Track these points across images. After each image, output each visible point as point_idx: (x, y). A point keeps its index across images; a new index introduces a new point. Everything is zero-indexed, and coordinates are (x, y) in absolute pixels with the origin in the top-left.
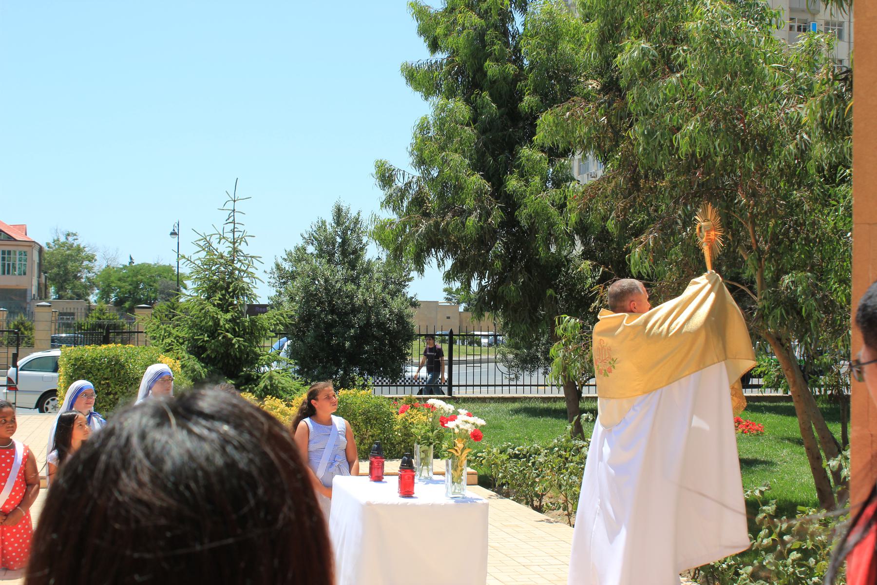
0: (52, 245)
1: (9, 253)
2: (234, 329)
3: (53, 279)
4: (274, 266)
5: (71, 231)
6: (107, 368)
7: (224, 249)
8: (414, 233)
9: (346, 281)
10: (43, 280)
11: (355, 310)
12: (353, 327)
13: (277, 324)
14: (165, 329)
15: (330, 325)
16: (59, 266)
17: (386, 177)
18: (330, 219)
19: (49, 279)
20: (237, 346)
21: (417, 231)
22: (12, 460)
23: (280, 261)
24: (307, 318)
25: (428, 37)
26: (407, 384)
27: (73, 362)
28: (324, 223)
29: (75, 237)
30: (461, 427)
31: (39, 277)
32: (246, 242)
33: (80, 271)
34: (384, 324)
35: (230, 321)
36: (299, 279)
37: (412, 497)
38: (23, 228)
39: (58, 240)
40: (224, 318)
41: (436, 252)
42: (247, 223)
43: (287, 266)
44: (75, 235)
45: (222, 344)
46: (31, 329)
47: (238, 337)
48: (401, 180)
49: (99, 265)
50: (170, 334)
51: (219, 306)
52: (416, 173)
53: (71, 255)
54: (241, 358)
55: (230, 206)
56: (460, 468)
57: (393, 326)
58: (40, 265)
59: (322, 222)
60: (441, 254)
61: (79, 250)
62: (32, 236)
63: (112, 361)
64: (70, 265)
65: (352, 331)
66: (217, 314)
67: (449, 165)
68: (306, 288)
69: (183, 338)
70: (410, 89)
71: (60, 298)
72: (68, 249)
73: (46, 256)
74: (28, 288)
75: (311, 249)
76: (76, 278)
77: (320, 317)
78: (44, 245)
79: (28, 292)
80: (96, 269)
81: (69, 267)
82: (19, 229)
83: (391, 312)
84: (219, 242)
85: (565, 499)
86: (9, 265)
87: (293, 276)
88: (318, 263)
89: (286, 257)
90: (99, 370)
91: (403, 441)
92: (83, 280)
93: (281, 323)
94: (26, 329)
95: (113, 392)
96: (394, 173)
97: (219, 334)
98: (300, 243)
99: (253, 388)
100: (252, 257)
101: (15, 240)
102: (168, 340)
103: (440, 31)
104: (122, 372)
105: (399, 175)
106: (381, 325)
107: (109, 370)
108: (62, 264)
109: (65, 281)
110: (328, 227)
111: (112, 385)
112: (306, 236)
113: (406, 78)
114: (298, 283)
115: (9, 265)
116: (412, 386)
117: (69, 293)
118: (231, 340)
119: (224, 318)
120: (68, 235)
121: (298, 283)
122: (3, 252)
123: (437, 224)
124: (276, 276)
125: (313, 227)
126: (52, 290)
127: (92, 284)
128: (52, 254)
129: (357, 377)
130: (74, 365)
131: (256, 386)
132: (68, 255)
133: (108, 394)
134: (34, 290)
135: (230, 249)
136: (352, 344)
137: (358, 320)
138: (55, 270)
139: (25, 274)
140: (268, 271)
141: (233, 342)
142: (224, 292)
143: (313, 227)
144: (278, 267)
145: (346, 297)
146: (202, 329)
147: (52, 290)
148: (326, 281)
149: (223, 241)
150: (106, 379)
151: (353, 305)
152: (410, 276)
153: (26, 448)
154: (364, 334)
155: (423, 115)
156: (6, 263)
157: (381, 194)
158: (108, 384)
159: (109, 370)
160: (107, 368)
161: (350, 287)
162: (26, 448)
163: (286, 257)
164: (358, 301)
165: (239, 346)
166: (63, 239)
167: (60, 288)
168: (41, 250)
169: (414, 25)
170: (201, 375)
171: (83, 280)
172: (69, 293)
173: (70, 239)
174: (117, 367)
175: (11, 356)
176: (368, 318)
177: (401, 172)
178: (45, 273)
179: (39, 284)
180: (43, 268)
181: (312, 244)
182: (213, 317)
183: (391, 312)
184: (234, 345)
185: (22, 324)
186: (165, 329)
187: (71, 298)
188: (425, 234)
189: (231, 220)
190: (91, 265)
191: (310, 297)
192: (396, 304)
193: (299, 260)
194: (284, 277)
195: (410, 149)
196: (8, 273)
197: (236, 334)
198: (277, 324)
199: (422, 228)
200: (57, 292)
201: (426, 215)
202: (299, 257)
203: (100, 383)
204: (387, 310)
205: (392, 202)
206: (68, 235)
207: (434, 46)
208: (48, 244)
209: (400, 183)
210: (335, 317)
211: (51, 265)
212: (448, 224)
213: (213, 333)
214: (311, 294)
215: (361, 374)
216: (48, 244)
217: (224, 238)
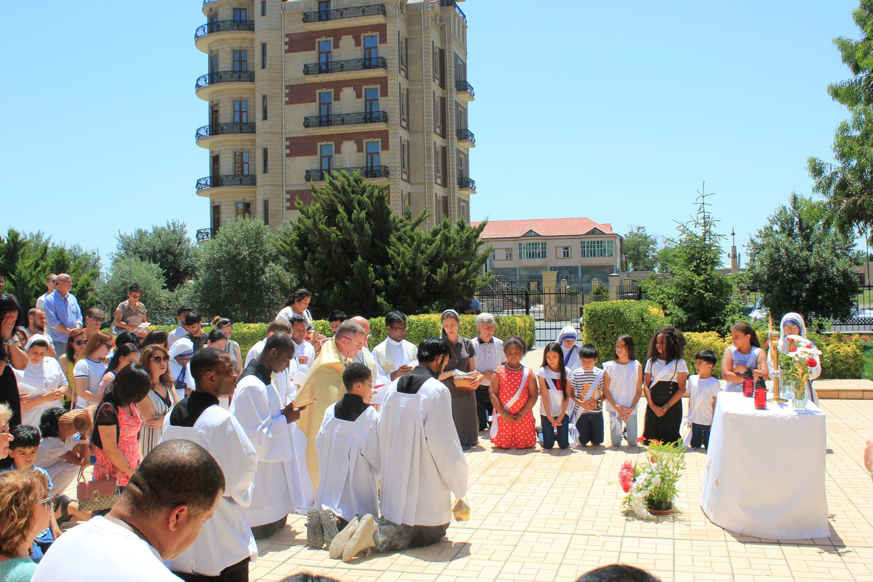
0: (628, 236)
1: (601, 242)
2: (706, 287)
3: (630, 258)
4: (749, 241)
5: (640, 226)
6: (611, 316)
7: (699, 232)
8: (837, 210)
9: (802, 249)
10: (624, 259)
11: (809, 270)
12: (808, 282)
13: (739, 282)
14: (660, 289)
15: (791, 282)
16: (634, 249)
17: (817, 170)
18: (789, 206)
19: (628, 258)
20: (707, 299)
21: (839, 208)
22: (522, 376)
23: (753, 237)
24: (774, 277)
25: (851, 62)
26: (867, 323)
27: (589, 312)
28: (784, 208)
29: (644, 230)
30: (800, 356)
31: (621, 257)
32: (714, 225)
33: (647, 252)
34: (833, 279)
35: (703, 281)
36: (766, 249)
37: (765, 409)
38: (609, 226)
39: (632, 232)
40: (697, 279)
41: (857, 224)
42: (714, 213)
43: (759, 241)
44: (643, 228)
45: (698, 298)
46: (607, 291)
47: (709, 292)
48: (829, 171)
49: (660, 246)
50: (663, 292)
51: (694, 271)
52: (838, 164)
53: (641, 241)
54: (711, 307)
55: (701, 200)
56: (801, 388)
57: (840, 280)
58: (621, 249)
59: (783, 207)
60: (861, 224)
61: (646, 237)
62: (615, 231)
63: (615, 311)
64: (641, 248)
65: (807, 285)
66: (692, 277)
67: (865, 156)
68: (771, 256)
69: (672, 294)
70: (837, 103)
71: (636, 270)
72: (639, 238)
73: (625, 243)
74: (615, 265)
75: (776, 228)
76: (645, 256)
77: (783, 276)
78: (623, 236)
79: (615, 267)
80: (657, 250)
81: (640, 250)
82: (607, 227)
83: (838, 270)
84: (696, 226)
85: (190, 444)
86: (601, 250)
87: (763, 247)
88: (782, 237)
89: (758, 234)
90: (606, 317)
91: (832, 366)
92: (650, 258)
93: (742, 282)
94: (604, 291)
95: (617, 332)
96: (823, 166)
97: (695, 291)
98: (768, 224)
99: (720, 328)
100: (719, 235)
101: (605, 234)
102: (662, 296)
103: (859, 54)
104: (622, 318)
105: (827, 168)
106: (830, 280)
107: (613, 317)
108: (636, 247)
109: (638, 259)
110: (788, 211)
111: (615, 327)
112: (771, 219)
113: (832, 95)
114: (764, 253)
115: (601, 250)
116: (853, 325)
117: (641, 267)
118: (704, 294)
119: (697, 279)
120: (639, 228)
121: (764, 253)
122: (582, 242)
123: (855, 202)
124: (751, 248)
125: (777, 212)
126: (630, 265)
127: (656, 260)
128: (629, 241)
129: (812, 319)
130: (590, 314)
131: (723, 326)
132: (639, 242)
133: (613, 333)
134: (618, 266)
135: (704, 231)
136: (807, 294)
137: (812, 277)
138: (632, 252)
139: (612, 255)
140: (746, 245)
141: (705, 296)
142: (698, 261)
143: (777, 212)
144: (752, 241)
145: (803, 261)
146: (684, 287)
147: (630, 265)
148: (786, 249)
149: (698, 225)
150: (611, 323)
151: (808, 266)
152: (854, 243)
153: (531, 371)
154: (817, 287)
155: (843, 120)
156: (600, 249)
157: (813, 182)
158: (613, 326)
159: (613, 317)
160: (611, 316)
161: (805, 253)
162: (531, 371)
163: (758, 234)
164: (812, 264)
165: (709, 298)
166: (635, 231)
167: (635, 264)
168: (621, 239)
169: (839, 55)
170: (683, 320)
171: (650, 258)
172: (641, 267)
173: (641, 231)
174: (618, 315)
175: (579, 309)
176: (820, 275)
177: (829, 165)
178: (625, 254)
179: (621, 262)
180: (624, 251)
181: (777, 224)
182: (690, 279)
183: (838, 270)
184: (706, 298)
185: (602, 288)
186: (660, 289)
187: (643, 270)
188: (845, 210)
189: (702, 210)
190: (654, 247)
191: (774, 262)
192: (841, 264)
193: (766, 236)
194: (758, 249)
195: (833, 147)
196: (601, 255)
197: (707, 290)
198: (739, 282)
199: (843, 206)
200: (633, 266)
201: (849, 196)
202: (767, 233)
203: (607, 326)
204: (834, 269)
205: (822, 187)
206: (639, 228)
207: (857, 69)
208: (626, 235)
209: (827, 173)
210: (794, 275)
211: (629, 249)
212: (863, 201)
213: (691, 291)
214: (776, 260)
215: (816, 316)
216: (626, 235)
217: (698, 223)
